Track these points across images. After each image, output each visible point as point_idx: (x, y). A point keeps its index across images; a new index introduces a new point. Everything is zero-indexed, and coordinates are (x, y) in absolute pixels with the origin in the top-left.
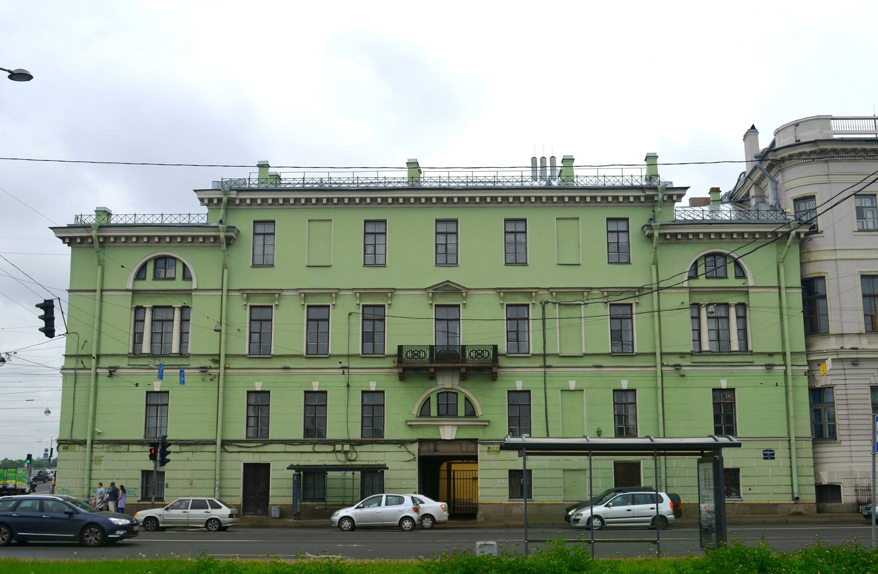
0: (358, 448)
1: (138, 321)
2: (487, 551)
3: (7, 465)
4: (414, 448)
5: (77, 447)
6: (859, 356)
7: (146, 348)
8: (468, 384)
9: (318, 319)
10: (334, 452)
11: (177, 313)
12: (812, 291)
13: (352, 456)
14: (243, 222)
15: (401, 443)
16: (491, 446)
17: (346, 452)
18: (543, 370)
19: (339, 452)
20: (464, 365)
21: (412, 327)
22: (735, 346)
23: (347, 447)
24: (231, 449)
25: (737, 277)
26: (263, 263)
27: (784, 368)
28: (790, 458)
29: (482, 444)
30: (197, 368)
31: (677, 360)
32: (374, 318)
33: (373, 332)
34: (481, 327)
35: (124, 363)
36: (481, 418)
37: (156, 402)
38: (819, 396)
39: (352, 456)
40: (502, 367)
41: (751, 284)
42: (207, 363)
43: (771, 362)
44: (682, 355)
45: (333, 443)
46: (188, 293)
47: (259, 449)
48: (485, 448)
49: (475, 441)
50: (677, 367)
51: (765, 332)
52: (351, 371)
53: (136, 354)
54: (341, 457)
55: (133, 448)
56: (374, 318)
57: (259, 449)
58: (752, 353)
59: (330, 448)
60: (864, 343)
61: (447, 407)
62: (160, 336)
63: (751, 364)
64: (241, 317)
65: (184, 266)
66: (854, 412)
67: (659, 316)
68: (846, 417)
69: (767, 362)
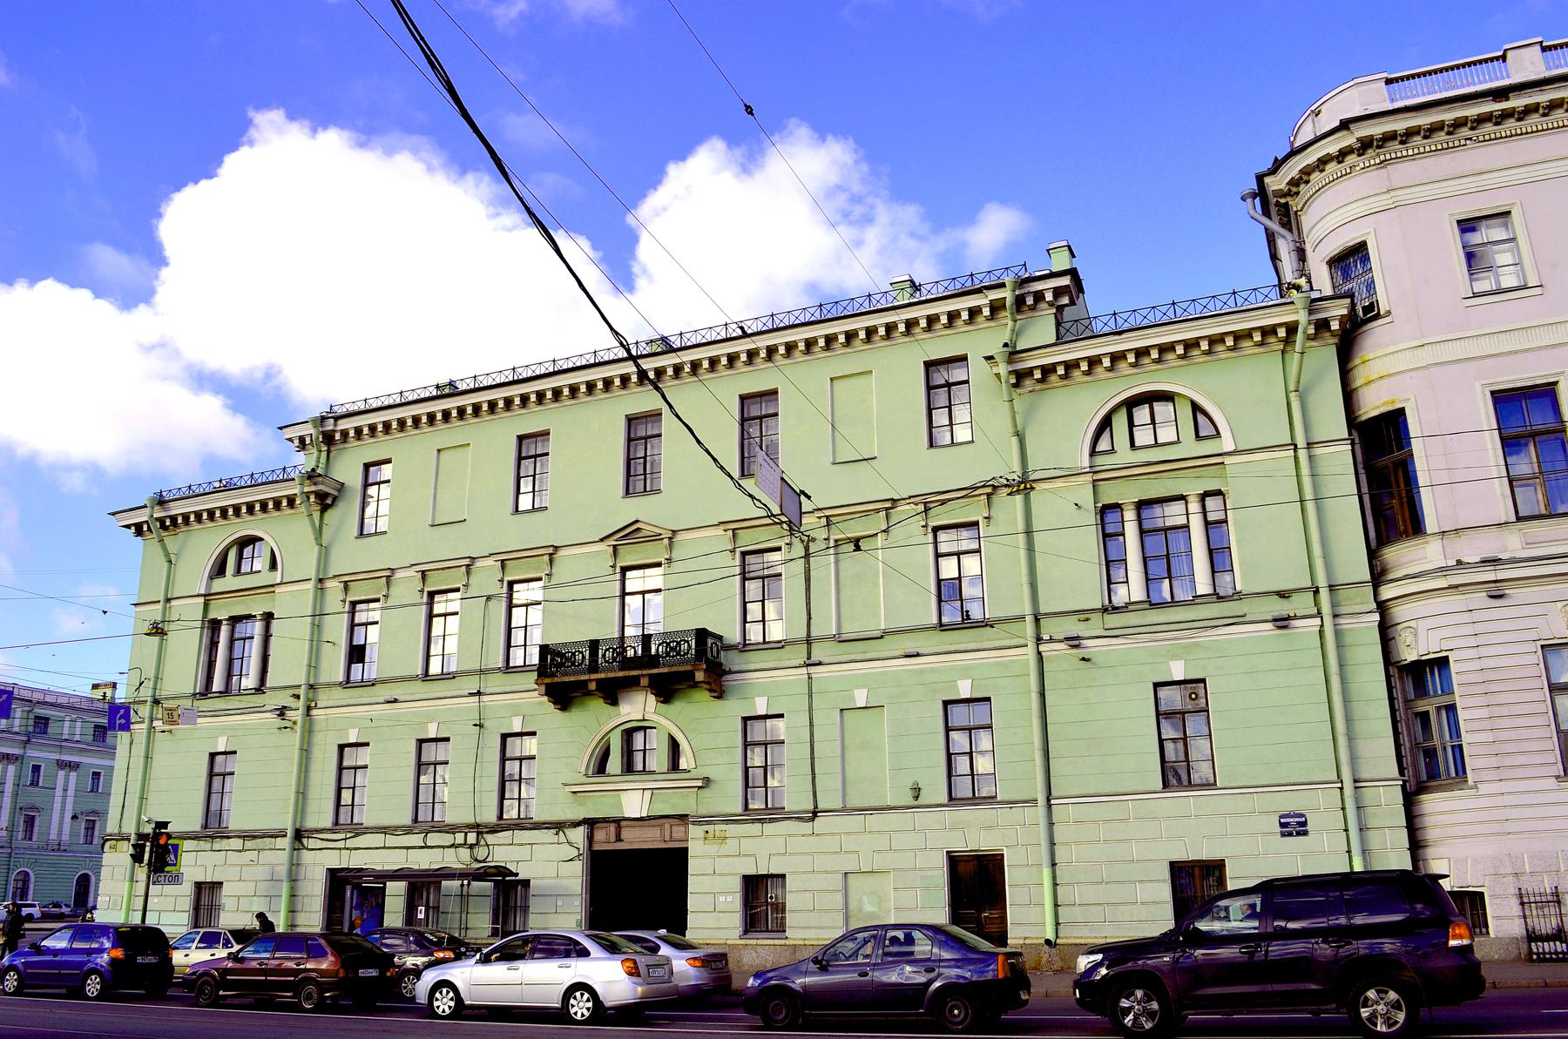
0: (490, 838)
1: (1109, 537)
4: (578, 835)
6: (1501, 575)
8: (677, 707)
11: (1130, 515)
12: (1382, 446)
13: (481, 853)
14: (347, 468)
15: (559, 826)
16: (710, 828)
18: (804, 670)
20: (594, 676)
24: (311, 843)
27: (1317, 621)
28: (1346, 830)
29: (694, 823)
31: (1072, 627)
33: (959, 578)
35: (1096, 625)
38: (1416, 681)
39: (481, 853)
40: (731, 672)
41: (1227, 444)
43: (1284, 613)
44: (1083, 614)
45: (452, 829)
47: (350, 843)
50: (1074, 641)
51: (1268, 548)
52: (484, 698)
53: (206, 692)
54: (465, 854)
57: (350, 843)
59: (447, 839)
60: (1513, 543)
61: (625, 754)
63: (1239, 620)
65: (1196, 408)
66: (1505, 711)
67: (837, 562)
68: (1487, 724)
69: (1277, 614)
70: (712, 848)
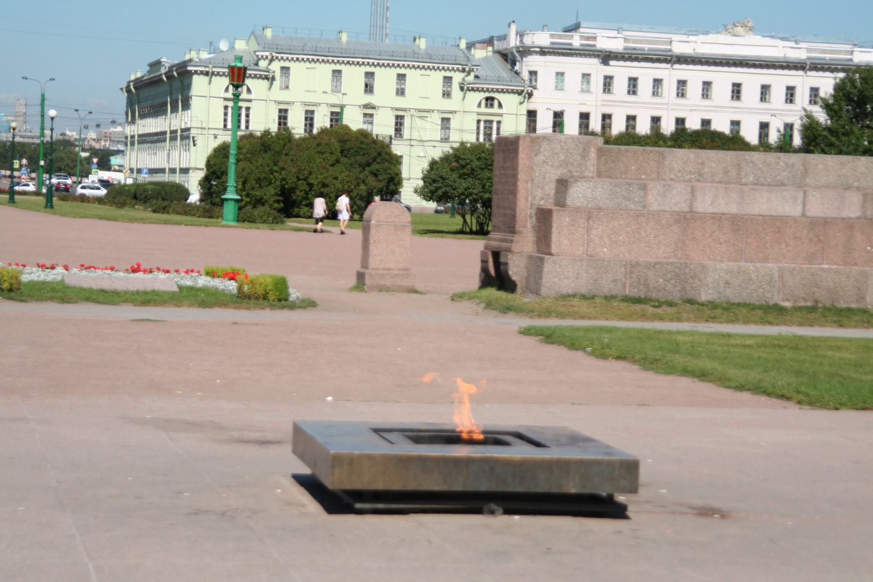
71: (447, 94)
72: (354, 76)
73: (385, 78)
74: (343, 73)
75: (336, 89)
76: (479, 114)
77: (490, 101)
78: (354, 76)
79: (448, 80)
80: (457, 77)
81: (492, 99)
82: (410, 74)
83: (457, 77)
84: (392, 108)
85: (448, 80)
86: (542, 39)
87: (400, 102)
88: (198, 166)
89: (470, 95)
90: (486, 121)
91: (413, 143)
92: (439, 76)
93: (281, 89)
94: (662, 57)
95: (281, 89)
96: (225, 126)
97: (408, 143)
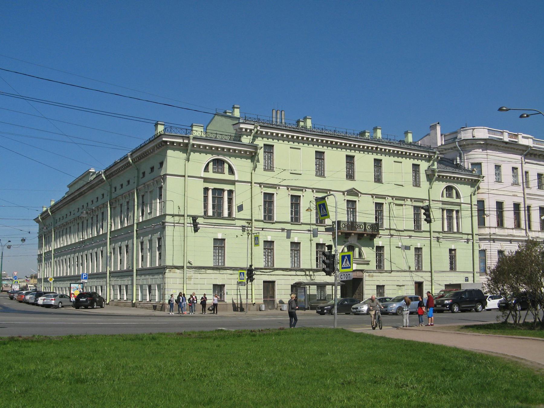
0: (315, 273)
2: (172, 186)
3: (543, 401)
5: (177, 271)
7: (210, 213)
9: (295, 201)
10: (306, 275)
17: (310, 276)
19: (307, 275)
21: (337, 212)
22: (455, 230)
23: (311, 273)
25: (457, 198)
26: (269, 168)
30: (240, 227)
32: (322, 208)
34: (365, 215)
36: (365, 260)
37: (219, 244)
42: (244, 223)
46: (233, 183)
47: (271, 273)
48: (367, 274)
49: (362, 271)
54: (308, 278)
55: (209, 271)
56: (322, 208)
57: (271, 273)
58: (462, 233)
59: (303, 273)
62: (218, 207)
63: (234, 225)
64: (260, 200)
70: (370, 279)
71: (417, 183)
72: (335, 158)
73: (364, 162)
74: (325, 153)
75: (320, 171)
76: (206, 180)
77: (218, 163)
78: (335, 158)
79: (416, 167)
80: (424, 166)
81: (222, 162)
82: (387, 161)
83: (424, 166)
84: (372, 195)
85: (416, 167)
86: (482, 133)
87: (379, 189)
88: (176, 264)
89: (194, 156)
90: (214, 190)
91: (392, 232)
92: (408, 163)
93: (265, 170)
94: (510, 150)
95: (265, 170)
96: (206, 212)
97: (387, 232)
